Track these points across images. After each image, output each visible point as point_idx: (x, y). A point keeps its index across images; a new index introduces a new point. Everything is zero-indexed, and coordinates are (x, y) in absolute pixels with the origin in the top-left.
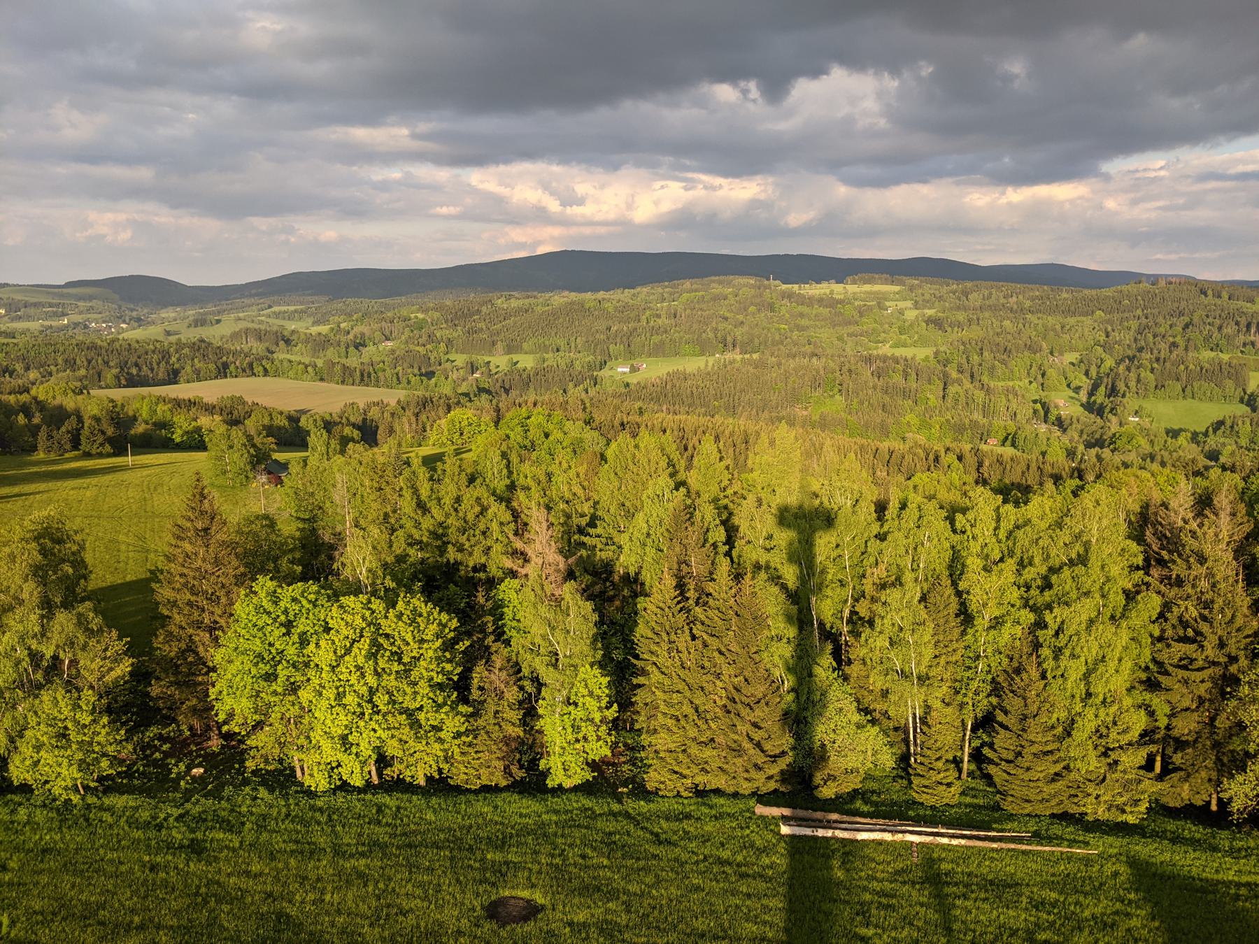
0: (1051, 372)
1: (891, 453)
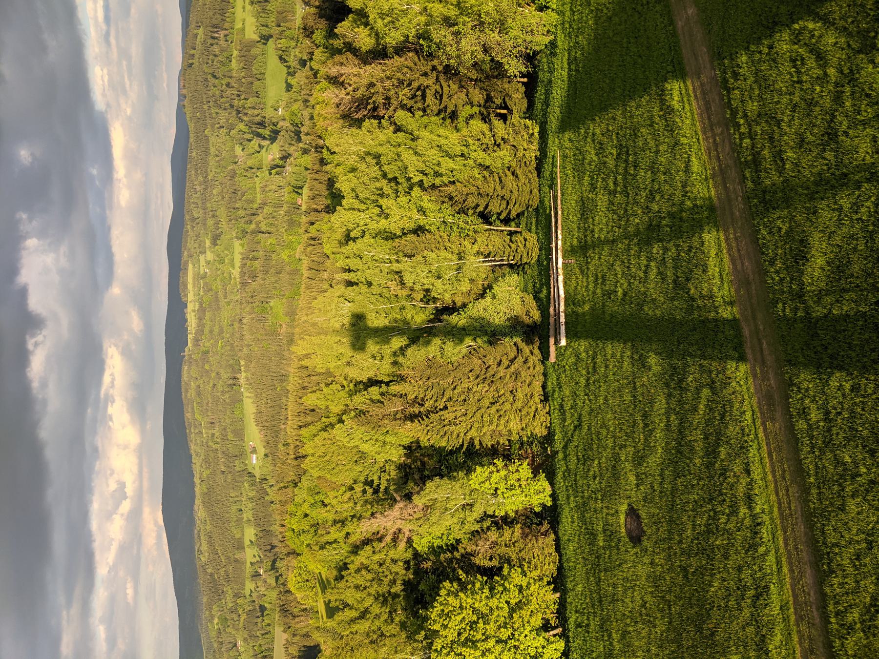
0: (250, 163)
1: (311, 269)
